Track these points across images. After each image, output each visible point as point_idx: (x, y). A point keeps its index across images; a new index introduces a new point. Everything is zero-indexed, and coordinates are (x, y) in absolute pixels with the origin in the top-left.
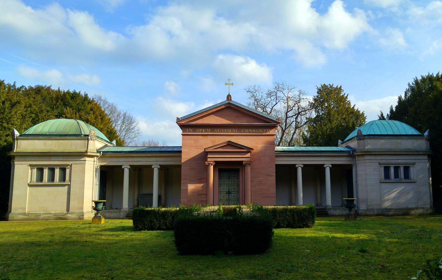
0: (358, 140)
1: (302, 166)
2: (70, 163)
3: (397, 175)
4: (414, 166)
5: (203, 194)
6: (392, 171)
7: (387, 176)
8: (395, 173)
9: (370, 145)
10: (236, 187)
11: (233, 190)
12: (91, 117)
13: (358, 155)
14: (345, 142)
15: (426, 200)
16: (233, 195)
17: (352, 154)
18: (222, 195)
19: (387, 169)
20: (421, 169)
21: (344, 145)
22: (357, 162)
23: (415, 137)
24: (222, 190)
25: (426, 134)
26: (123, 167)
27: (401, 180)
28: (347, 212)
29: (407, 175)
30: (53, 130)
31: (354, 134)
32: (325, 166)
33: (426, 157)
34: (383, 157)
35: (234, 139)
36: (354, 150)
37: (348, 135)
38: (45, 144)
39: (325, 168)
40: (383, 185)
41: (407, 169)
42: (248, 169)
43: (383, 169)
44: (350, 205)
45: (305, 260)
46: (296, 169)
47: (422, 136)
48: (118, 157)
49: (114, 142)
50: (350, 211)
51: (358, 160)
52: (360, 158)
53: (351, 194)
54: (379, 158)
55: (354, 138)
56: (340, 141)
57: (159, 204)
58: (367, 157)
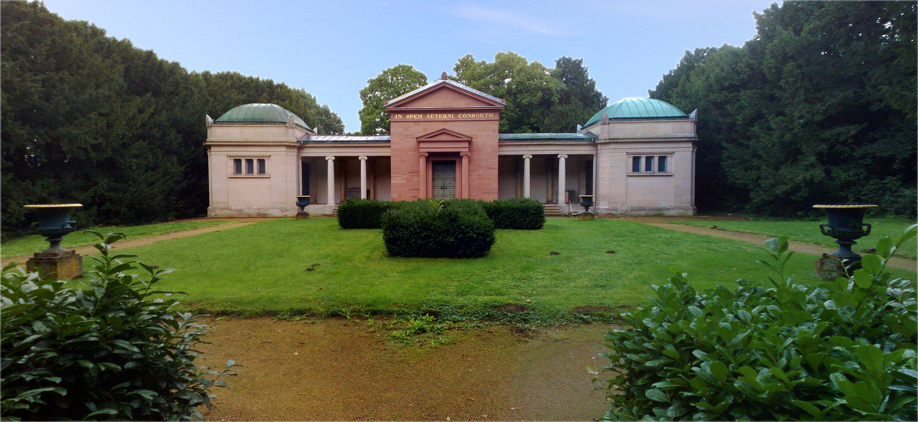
3: (648, 168)
6: (643, 161)
7: (636, 167)
8: (649, 163)
12: (234, 95)
13: (601, 144)
19: (636, 160)
20: (682, 162)
21: (585, 131)
25: (693, 115)
29: (662, 167)
33: (690, 145)
35: (449, 127)
36: (596, 138)
40: (631, 179)
41: (662, 159)
42: (465, 161)
43: (631, 160)
45: (348, 283)
49: (316, 130)
50: (587, 210)
52: (604, 147)
53: (589, 190)
54: (628, 146)
56: (579, 127)
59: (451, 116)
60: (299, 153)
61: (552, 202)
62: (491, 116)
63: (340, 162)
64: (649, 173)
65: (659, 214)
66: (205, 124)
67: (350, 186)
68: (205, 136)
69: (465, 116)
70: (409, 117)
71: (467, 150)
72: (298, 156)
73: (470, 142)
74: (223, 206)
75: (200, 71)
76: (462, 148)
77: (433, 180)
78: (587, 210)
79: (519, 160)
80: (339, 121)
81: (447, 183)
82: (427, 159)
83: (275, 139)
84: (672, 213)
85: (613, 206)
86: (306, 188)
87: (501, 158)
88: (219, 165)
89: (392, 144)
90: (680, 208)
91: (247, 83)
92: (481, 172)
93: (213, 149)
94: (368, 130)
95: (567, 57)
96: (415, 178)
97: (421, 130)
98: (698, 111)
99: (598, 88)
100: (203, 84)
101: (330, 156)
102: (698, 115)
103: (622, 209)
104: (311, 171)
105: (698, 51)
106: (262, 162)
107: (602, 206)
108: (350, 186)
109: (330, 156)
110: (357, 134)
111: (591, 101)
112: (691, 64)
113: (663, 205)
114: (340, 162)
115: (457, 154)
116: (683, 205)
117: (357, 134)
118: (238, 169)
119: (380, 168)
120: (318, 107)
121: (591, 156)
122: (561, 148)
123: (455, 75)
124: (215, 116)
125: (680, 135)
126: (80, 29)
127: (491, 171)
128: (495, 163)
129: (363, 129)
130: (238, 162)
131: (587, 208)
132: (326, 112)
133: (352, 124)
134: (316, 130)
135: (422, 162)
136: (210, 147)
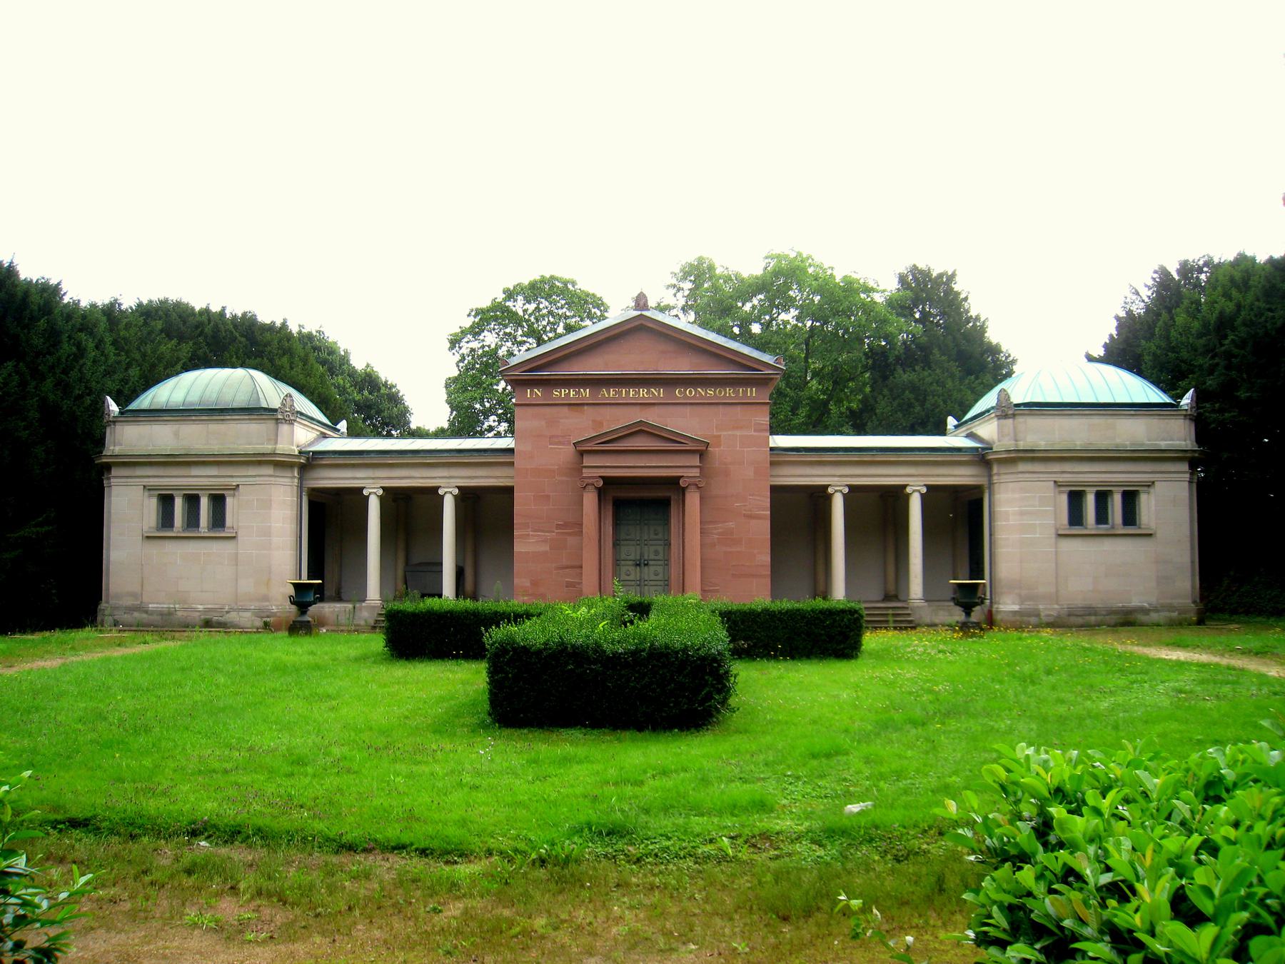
0: (999, 417)
1: (846, 490)
2: (234, 482)
3: (1102, 517)
4: (1152, 490)
5: (572, 567)
7: (1076, 516)
9: (1039, 433)
10: (660, 549)
11: (652, 557)
14: (966, 422)
15: (1183, 585)
16: (652, 569)
17: (982, 458)
18: (624, 569)
19: (1076, 498)
20: (1170, 505)
22: (995, 478)
23: (1156, 411)
24: (623, 556)
25: (1186, 400)
26: (365, 492)
27: (1113, 527)
28: (958, 615)
29: (1130, 516)
30: (194, 399)
31: (989, 400)
32: (908, 490)
34: (1068, 467)
35: (653, 417)
37: (970, 407)
38: (176, 435)
39: (908, 496)
41: (1130, 498)
42: (693, 499)
43: (1064, 499)
44: (968, 598)
46: (828, 499)
47: (1174, 406)
48: (353, 466)
49: (343, 426)
50: (968, 614)
51: (998, 474)
53: (977, 571)
54: (1057, 467)
55: (988, 411)
56: (951, 421)
57: (460, 590)
58: (1022, 467)
59: (658, 393)
60: (301, 479)
61: (895, 597)
62: (752, 392)
63: (396, 501)
64: (1076, 530)
65: (1126, 620)
66: (102, 417)
67: (417, 558)
68: (100, 442)
69: (690, 392)
70: (560, 393)
71: (696, 472)
72: (301, 487)
73: (702, 454)
74: (129, 602)
75: (102, 299)
76: (684, 467)
77: (616, 544)
78: (968, 614)
79: (819, 496)
80: (395, 399)
81: (649, 553)
82: (601, 492)
83: (250, 448)
84: (1154, 617)
85: (1028, 605)
86: (317, 565)
87: (778, 492)
88: (127, 508)
89: (516, 459)
90: (1171, 608)
91: (199, 325)
92: (731, 525)
93: (114, 472)
94: (465, 423)
95: (922, 266)
96: (571, 541)
97: (582, 425)
98: (1196, 391)
99: (993, 336)
100: (103, 324)
101: (373, 486)
102: (1200, 398)
103: (1048, 609)
104: (330, 521)
105: (1186, 269)
106: (218, 501)
107: (1007, 605)
108: (417, 558)
109: (373, 486)
110: (440, 434)
111: (979, 364)
112: (1172, 292)
113: (1135, 602)
114: (396, 501)
115: (673, 482)
116: (1175, 602)
117: (440, 434)
118: (166, 519)
119: (487, 514)
120: (352, 373)
121: (978, 489)
122: (912, 470)
123: (669, 299)
124: (124, 398)
125: (1163, 444)
126: (147, 313)
127: (753, 522)
128: (762, 504)
129: (452, 423)
130: (166, 501)
131: (968, 609)
132: (369, 381)
133: (429, 408)
134: (343, 426)
135: (590, 499)
136: (108, 467)
